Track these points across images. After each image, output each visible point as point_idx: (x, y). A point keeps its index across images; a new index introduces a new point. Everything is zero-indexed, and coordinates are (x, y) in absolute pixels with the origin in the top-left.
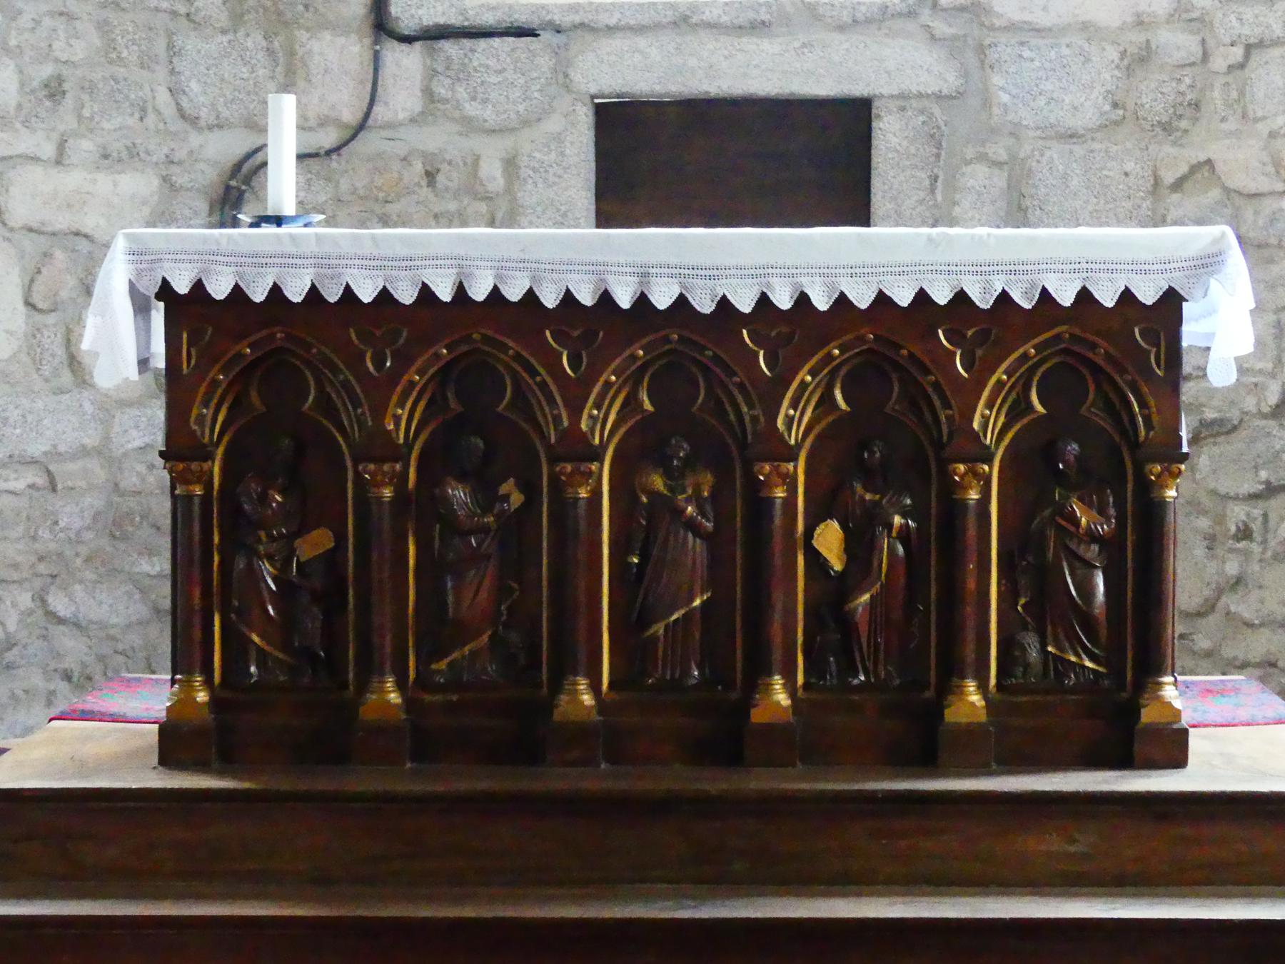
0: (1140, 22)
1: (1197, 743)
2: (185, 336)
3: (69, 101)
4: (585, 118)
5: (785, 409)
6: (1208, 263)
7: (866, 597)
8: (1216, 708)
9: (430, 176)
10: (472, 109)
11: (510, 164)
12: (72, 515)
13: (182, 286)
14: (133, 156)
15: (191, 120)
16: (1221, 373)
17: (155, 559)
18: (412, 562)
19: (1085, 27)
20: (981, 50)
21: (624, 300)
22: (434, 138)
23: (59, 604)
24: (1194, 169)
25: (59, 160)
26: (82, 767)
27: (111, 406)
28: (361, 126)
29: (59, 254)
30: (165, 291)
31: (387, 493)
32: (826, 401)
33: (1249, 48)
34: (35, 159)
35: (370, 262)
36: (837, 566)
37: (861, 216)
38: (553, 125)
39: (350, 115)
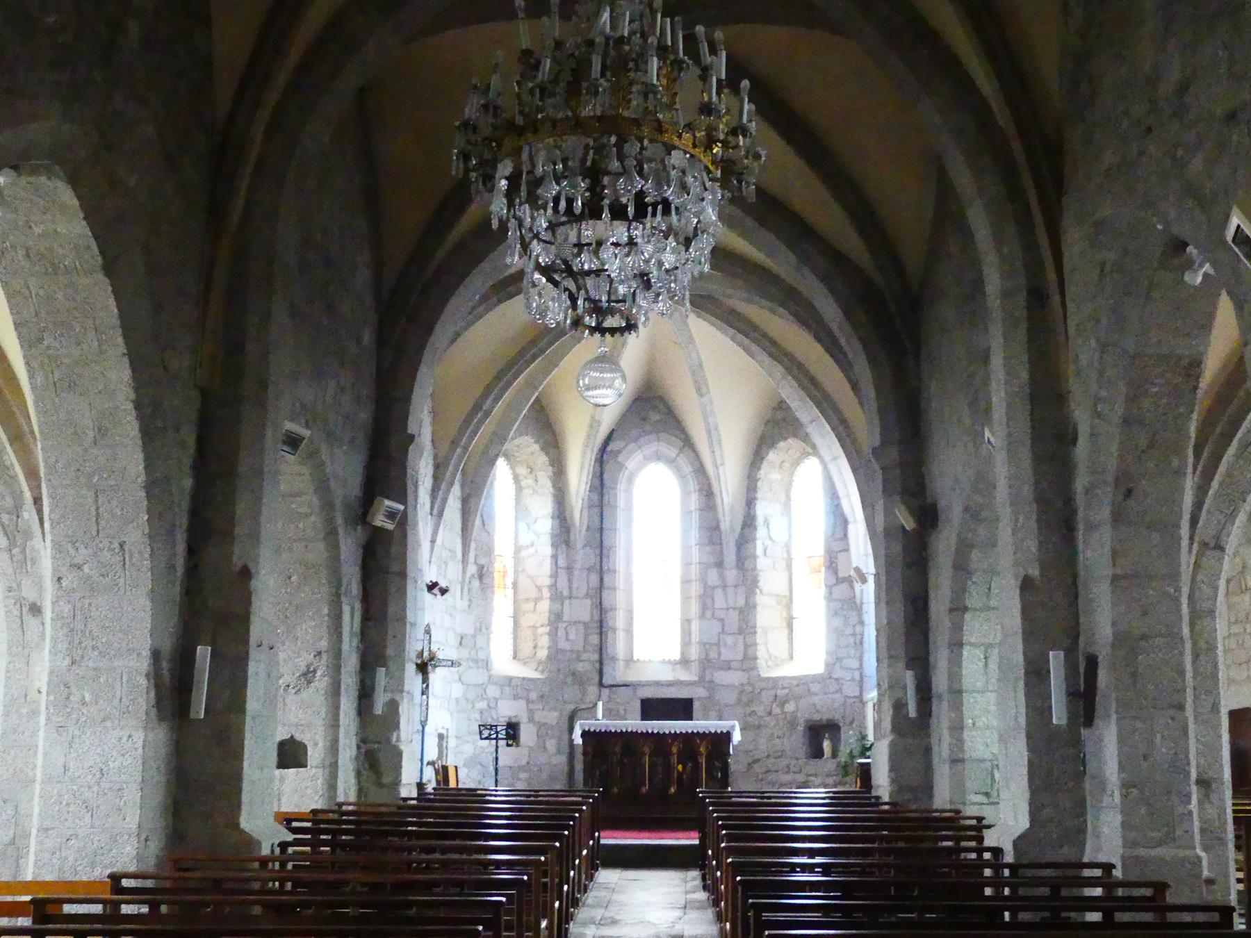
0: (742, 685)
2: (927, 915)
4: (639, 702)
10: (618, 700)
14: (555, 709)
18: (854, 932)
21: (650, 732)
35: (614, 726)
37: (691, 719)
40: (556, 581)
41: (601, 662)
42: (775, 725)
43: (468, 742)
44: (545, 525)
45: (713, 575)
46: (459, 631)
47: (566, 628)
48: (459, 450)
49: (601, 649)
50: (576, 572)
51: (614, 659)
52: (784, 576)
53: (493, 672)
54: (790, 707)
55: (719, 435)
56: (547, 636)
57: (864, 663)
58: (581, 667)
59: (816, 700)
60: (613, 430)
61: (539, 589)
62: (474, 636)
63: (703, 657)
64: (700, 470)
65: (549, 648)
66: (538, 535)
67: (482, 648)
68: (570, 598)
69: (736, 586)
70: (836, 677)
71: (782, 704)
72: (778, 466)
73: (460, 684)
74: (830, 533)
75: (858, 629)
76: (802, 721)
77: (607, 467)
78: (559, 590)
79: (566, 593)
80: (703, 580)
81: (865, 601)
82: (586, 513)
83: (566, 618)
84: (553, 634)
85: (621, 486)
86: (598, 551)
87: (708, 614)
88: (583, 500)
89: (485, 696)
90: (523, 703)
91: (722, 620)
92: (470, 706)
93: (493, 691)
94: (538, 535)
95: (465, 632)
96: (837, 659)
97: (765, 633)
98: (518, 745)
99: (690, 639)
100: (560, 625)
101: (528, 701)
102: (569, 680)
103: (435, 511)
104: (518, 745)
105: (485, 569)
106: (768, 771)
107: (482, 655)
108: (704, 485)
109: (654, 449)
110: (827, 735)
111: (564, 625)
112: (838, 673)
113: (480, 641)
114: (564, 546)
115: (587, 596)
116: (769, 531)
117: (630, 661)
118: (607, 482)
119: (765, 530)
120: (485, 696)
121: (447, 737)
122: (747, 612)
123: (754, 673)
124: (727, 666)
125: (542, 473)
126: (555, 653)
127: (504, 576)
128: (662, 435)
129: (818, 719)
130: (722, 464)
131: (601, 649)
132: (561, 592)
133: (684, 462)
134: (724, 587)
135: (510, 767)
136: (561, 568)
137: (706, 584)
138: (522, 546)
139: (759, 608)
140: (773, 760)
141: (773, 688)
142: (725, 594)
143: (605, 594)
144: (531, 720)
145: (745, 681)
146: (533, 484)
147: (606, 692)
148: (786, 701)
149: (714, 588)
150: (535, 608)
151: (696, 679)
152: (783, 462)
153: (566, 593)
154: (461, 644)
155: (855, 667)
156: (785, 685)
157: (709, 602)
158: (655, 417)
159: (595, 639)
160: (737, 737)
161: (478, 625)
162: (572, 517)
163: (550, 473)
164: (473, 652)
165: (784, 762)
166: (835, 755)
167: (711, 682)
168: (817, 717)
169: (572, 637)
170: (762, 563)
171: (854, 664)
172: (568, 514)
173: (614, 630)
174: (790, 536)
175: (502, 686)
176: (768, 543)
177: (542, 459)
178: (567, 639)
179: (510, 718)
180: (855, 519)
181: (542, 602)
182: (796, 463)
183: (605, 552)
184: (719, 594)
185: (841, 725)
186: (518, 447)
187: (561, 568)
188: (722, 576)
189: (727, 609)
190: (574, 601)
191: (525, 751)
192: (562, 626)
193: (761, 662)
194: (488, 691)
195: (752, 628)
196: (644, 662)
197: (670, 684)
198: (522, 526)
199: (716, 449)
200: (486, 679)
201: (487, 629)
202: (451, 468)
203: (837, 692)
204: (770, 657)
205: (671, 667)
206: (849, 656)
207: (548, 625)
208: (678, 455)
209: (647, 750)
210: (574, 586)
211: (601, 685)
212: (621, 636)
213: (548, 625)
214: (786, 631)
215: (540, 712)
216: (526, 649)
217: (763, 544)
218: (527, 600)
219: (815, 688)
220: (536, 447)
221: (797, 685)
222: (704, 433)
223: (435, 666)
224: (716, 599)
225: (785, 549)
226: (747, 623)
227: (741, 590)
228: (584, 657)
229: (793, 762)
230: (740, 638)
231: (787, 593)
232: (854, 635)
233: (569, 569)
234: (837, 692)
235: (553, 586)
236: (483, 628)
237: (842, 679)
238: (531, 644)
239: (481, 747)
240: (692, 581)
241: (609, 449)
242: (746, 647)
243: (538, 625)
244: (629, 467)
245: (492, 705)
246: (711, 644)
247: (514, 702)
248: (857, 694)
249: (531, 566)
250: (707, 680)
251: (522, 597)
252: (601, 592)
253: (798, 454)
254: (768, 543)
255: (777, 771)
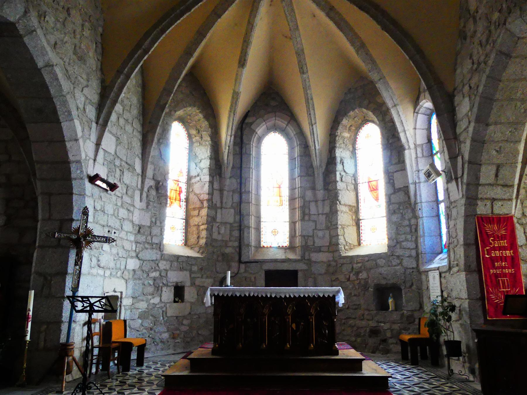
1: (340, 352)
3: (203, 271)
4: (264, 272)
5: (288, 309)
6: (338, 292)
7: (298, 333)
8: (342, 347)
9: (246, 279)
11: (255, 278)
12: (202, 321)
13: (216, 294)
15: (217, 272)
16: (340, 305)
17: (183, 102)
19: (322, 262)
20: (310, 264)
22: (246, 275)
23: (200, 332)
24: (336, 278)
25: (202, 277)
26: (202, 355)
27: (207, 308)
28: (238, 273)
29: (201, 289)
30: (214, 295)
31: (240, 320)
32: (293, 309)
33: (342, 265)
34: (199, 277)
36: (295, 329)
38: (260, 273)
39: (236, 272)
40: (212, 198)
41: (240, 247)
42: (352, 288)
43: (143, 301)
44: (206, 163)
45: (309, 194)
46: (137, 222)
47: (218, 227)
48: (122, 77)
49: (240, 240)
50: (225, 193)
51: (248, 245)
52: (352, 194)
53: (165, 252)
54: (363, 275)
55: (313, 103)
56: (205, 231)
57: (419, 244)
58: (228, 250)
59: (383, 270)
60: (249, 111)
61: (202, 202)
62: (150, 227)
63: (304, 244)
64: (301, 134)
65: (207, 238)
66: (202, 170)
67: (156, 235)
68: (221, 208)
69: (323, 201)
70: (397, 254)
71: (357, 274)
72: (348, 128)
73: (137, 260)
74: (387, 161)
75: (413, 221)
76: (373, 285)
77: (245, 132)
78: (214, 202)
79: (219, 205)
80: (303, 197)
81: (419, 201)
82: (231, 157)
83: (219, 219)
84: (209, 230)
85: (254, 144)
86: (239, 180)
87: (307, 218)
88: (229, 147)
89: (157, 268)
90: (187, 273)
91: (315, 221)
92: (145, 275)
93: (163, 265)
94: (202, 170)
95: (143, 224)
96: (397, 242)
97: (343, 228)
98: (183, 301)
99: (295, 233)
100: (214, 224)
101: (191, 272)
102: (220, 258)
103: (101, 121)
104: (183, 301)
105: (161, 184)
106: (348, 318)
107: (155, 240)
108: (303, 142)
109: (273, 122)
110: (391, 295)
111: (218, 224)
112: (399, 252)
113: (155, 231)
114: (218, 177)
115: (232, 207)
116: (343, 167)
117: (258, 247)
118: (245, 141)
119: (341, 166)
120: (157, 268)
121: (121, 298)
122: (333, 213)
123: (336, 254)
124: (319, 250)
125: (205, 133)
126: (211, 242)
127: (180, 194)
128: (277, 114)
129: (384, 283)
130: (315, 123)
131: (240, 240)
132: (216, 204)
133: (291, 130)
134: (316, 201)
135: (177, 317)
136: (216, 190)
137: (304, 200)
138: (192, 177)
139: (339, 213)
140: (352, 311)
141: (351, 263)
142: (317, 206)
143: (243, 205)
144: (193, 284)
145: (331, 259)
146: (200, 140)
147: (243, 266)
148: (360, 272)
149: (310, 202)
150: (199, 214)
151: (299, 258)
152: (351, 126)
153: (219, 205)
154: (139, 231)
155: (412, 247)
156: (359, 261)
157: (307, 211)
158: (273, 103)
159: (236, 233)
160: (341, 299)
161: (154, 220)
162: (223, 159)
163: (209, 132)
164: (149, 238)
165: (360, 312)
166: (398, 307)
167: (309, 260)
168: (383, 282)
169: (222, 232)
170: (340, 185)
171: (412, 245)
172: (220, 158)
173: (249, 227)
174: (356, 171)
175: (171, 262)
176: (343, 173)
177: (205, 124)
178: (219, 233)
179: (177, 283)
180: (409, 147)
181: (203, 210)
182: (359, 127)
183: (243, 181)
184: (313, 205)
185: (403, 288)
186: (190, 116)
187: (216, 190)
188: (315, 195)
189: (319, 214)
190: (224, 210)
191: (188, 305)
192: (215, 225)
193: (341, 247)
194: (160, 265)
195: (334, 225)
196: (267, 247)
197: (283, 261)
198: (193, 165)
199: (312, 112)
200: (159, 257)
201: (161, 223)
202: (115, 89)
203: (398, 265)
204: (347, 243)
205: (283, 251)
206: (406, 240)
207: (206, 224)
208: (287, 125)
209: (266, 311)
210: (224, 201)
211: (240, 262)
212: (253, 232)
213: (206, 224)
214: (355, 228)
215: (199, 279)
216: (193, 240)
217: (340, 174)
218: (194, 209)
219: (381, 262)
220: (201, 116)
221: (368, 261)
222: (303, 101)
223: (89, 243)
224: (311, 209)
225: (353, 178)
226: (331, 222)
227: (327, 203)
228: (230, 244)
229: (366, 313)
230: (327, 232)
231: (355, 205)
232: (410, 226)
233: (221, 191)
234: (398, 265)
235: (210, 200)
236: (158, 222)
237: (402, 256)
238: (195, 236)
239: (154, 304)
240: (297, 198)
241: (246, 121)
242: (331, 237)
243: (200, 224)
244: (258, 133)
245: (163, 274)
246: (308, 236)
247: (181, 273)
248: (415, 266)
249: (197, 188)
250: (306, 258)
251: (191, 207)
252: (240, 205)
253: (360, 121)
254: (343, 173)
255: (355, 318)
